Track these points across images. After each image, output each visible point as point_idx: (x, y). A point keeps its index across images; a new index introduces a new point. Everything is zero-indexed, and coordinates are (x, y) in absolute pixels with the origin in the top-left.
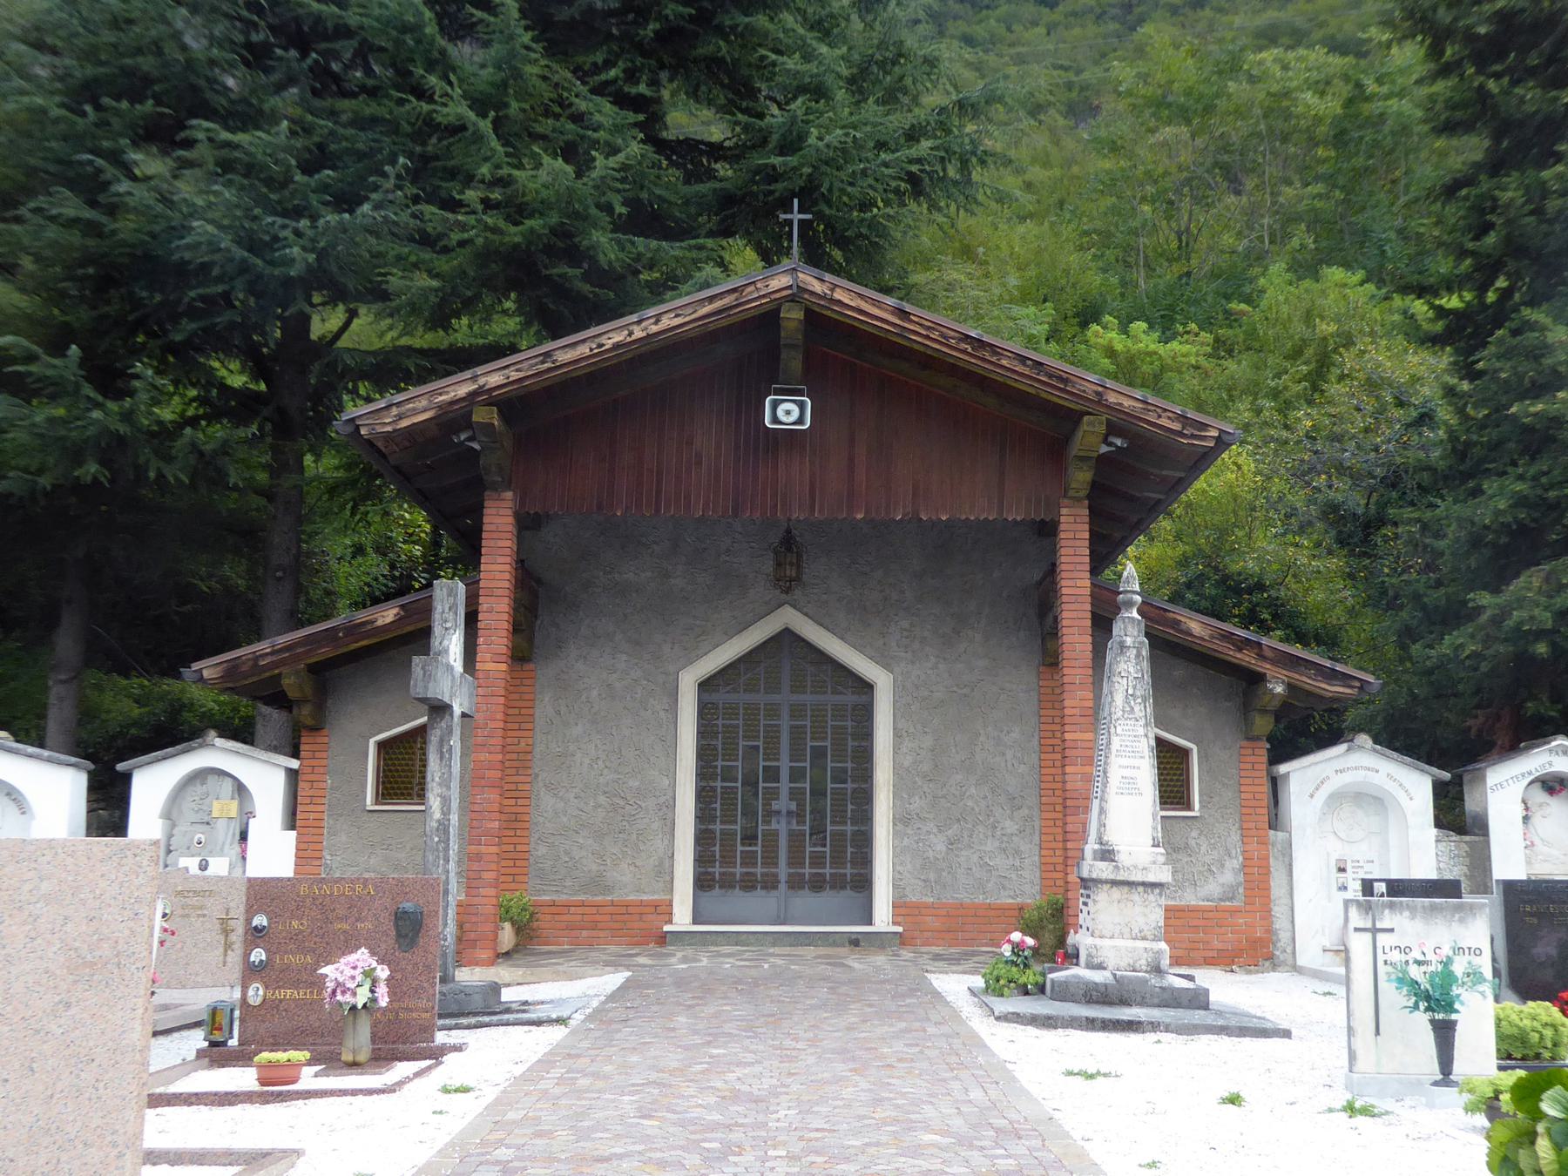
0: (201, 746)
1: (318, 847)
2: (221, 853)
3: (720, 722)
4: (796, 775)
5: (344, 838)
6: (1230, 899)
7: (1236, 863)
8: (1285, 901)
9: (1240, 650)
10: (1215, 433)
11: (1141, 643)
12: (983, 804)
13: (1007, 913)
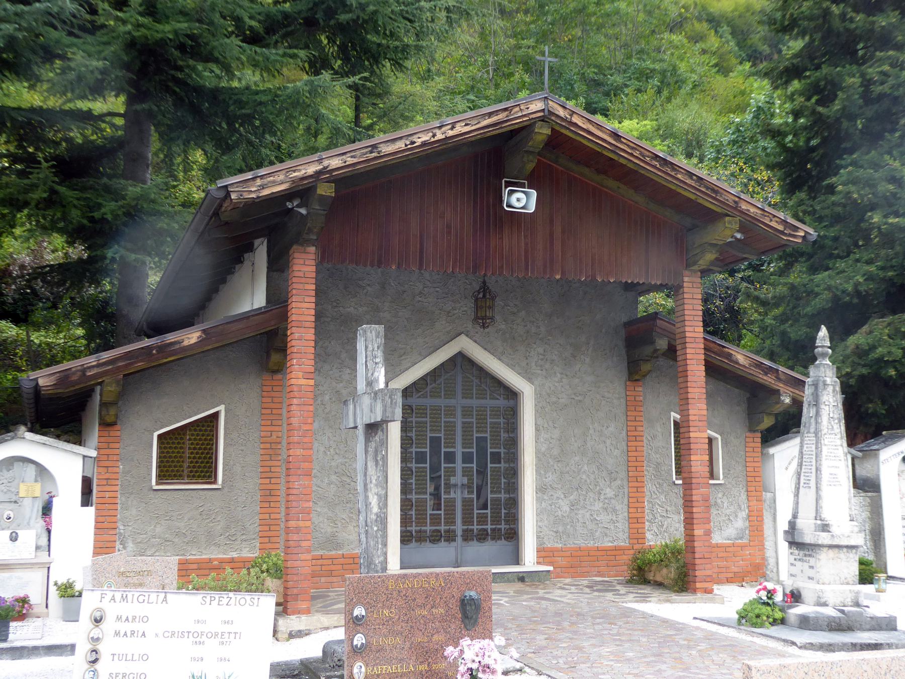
0: (13, 438)
1: (114, 519)
2: (28, 526)
3: (414, 420)
4: (467, 458)
5: (134, 512)
6: (741, 538)
7: (743, 514)
8: (772, 538)
9: (766, 374)
10: (802, 234)
11: (835, 382)
12: (592, 477)
13: (609, 553)
